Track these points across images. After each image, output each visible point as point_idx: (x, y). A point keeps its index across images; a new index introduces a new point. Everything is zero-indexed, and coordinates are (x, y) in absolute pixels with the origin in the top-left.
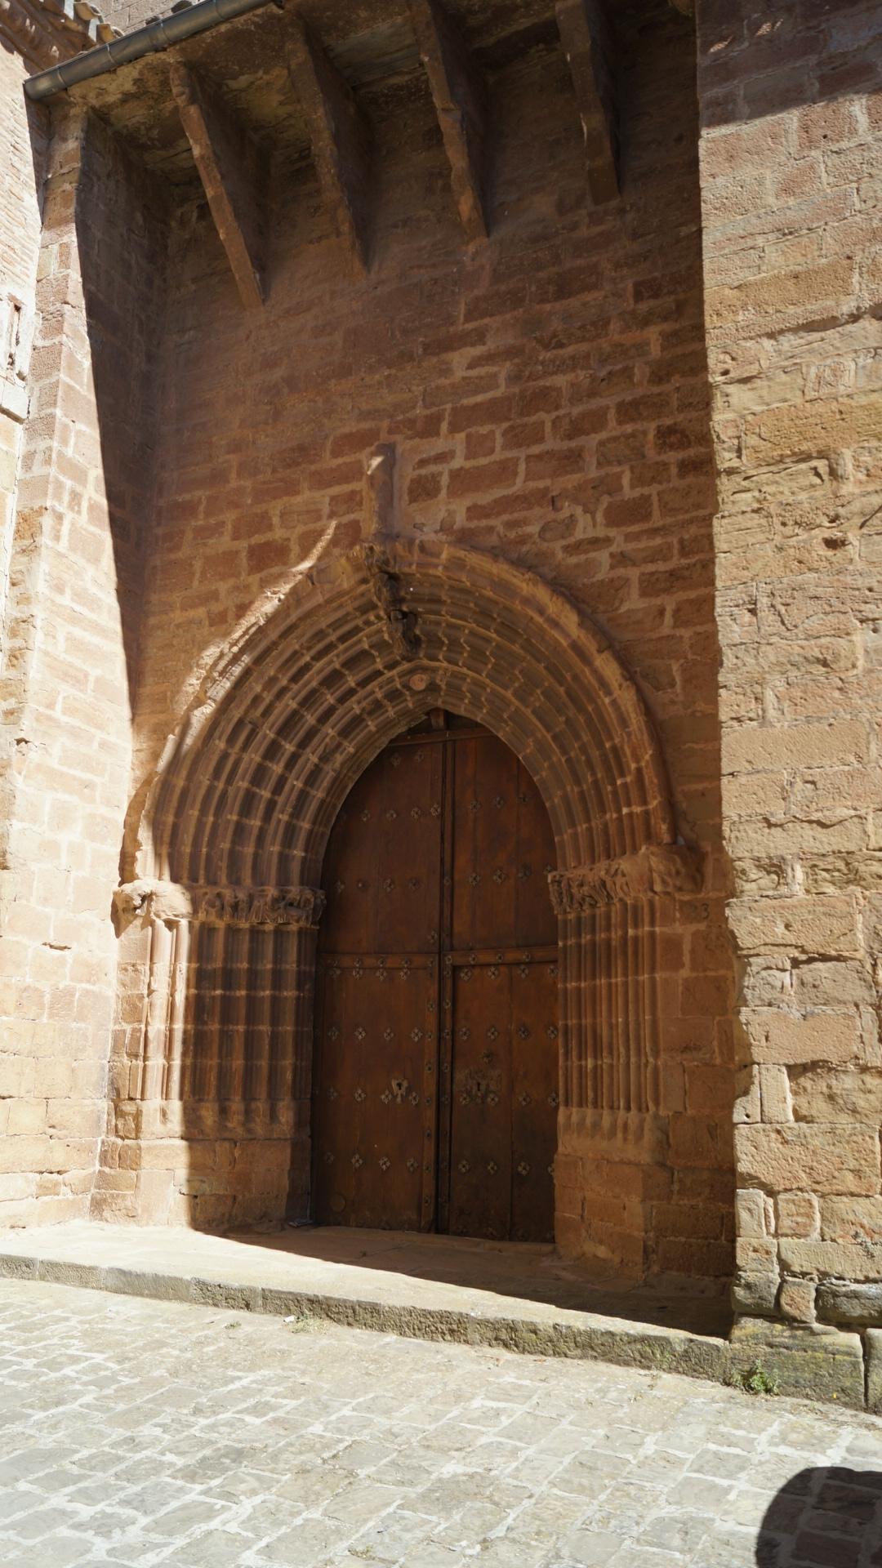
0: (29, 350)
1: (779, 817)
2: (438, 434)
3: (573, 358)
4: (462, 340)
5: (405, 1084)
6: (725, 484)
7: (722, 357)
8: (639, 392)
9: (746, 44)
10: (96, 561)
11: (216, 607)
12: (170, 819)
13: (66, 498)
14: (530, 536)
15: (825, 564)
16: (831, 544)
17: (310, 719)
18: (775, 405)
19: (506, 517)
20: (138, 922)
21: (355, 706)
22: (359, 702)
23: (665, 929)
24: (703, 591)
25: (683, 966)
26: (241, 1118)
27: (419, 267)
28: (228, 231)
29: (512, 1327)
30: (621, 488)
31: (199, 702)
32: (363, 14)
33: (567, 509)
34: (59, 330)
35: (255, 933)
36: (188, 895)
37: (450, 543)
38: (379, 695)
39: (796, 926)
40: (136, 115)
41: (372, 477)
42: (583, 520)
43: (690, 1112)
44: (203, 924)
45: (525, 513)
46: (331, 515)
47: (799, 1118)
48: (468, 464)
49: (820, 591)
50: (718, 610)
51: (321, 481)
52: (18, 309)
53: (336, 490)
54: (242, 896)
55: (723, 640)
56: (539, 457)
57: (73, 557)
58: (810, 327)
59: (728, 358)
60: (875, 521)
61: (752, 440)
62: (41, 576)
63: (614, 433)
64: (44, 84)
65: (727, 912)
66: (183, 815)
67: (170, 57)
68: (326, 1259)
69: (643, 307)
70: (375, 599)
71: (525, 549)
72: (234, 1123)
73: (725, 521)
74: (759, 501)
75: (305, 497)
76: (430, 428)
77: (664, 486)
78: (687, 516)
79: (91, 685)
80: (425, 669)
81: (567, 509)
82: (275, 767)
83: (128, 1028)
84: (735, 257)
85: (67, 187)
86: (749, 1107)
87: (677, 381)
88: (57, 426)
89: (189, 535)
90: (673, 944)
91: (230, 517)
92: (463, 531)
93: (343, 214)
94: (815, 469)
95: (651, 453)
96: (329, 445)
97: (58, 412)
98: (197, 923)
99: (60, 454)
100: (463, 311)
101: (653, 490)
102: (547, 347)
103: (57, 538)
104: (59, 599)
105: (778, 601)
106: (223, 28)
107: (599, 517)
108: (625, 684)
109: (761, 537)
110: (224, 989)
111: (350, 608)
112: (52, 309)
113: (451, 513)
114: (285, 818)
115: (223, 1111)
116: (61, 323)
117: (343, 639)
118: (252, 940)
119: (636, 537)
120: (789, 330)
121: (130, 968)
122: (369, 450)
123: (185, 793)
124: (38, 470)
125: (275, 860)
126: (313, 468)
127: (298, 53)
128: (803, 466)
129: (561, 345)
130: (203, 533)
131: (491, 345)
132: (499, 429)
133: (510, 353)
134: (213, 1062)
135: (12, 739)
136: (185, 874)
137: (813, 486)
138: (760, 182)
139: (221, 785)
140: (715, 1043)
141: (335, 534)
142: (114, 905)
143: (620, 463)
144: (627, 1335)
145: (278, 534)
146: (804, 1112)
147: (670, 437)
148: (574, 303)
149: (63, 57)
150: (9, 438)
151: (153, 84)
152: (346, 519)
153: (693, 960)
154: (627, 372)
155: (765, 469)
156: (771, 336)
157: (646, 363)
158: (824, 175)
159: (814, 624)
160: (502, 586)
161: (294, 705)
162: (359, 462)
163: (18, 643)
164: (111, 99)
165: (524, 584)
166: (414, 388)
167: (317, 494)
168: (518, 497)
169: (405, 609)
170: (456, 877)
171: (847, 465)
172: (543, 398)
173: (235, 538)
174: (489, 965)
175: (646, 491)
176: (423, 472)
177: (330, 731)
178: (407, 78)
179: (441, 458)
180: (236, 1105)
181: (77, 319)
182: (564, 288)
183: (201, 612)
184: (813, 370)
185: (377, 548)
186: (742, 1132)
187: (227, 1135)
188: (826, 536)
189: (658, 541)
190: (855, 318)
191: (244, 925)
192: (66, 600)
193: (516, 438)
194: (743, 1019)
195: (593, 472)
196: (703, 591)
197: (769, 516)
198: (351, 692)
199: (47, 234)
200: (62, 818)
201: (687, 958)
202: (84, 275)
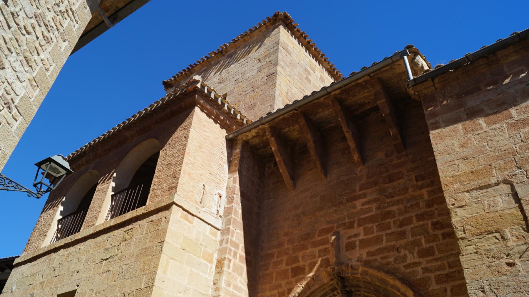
0: (223, 208)
2: (353, 228)
3: (397, 201)
6: (461, 243)
7: (451, 199)
8: (423, 211)
10: (241, 275)
11: (281, 290)
13: (232, 254)
14: (390, 262)
15: (509, 272)
16: (509, 265)
18: (474, 215)
19: (381, 255)
24: (460, 282)
28: (283, 170)
30: (422, 244)
32: (320, 110)
33: (403, 252)
34: (232, 202)
37: (362, 265)
40: (256, 141)
41: (332, 243)
45: (388, 254)
46: (319, 257)
48: (365, 238)
49: (509, 283)
50: (469, 291)
51: (315, 244)
52: (220, 197)
53: (320, 248)
56: (390, 234)
57: (234, 274)
58: (481, 188)
59: (453, 200)
60: (525, 255)
61: (469, 227)
62: (223, 281)
63: (416, 225)
64: (231, 136)
67: (266, 126)
69: (419, 183)
70: (336, 286)
71: (389, 267)
74: (476, 249)
75: (310, 250)
76: (351, 226)
77: (438, 243)
78: (448, 253)
81: (403, 252)
84: (449, 168)
85: (236, 162)
87: (436, 206)
88: (231, 231)
89: (271, 265)
91: (285, 258)
92: (366, 261)
93: (318, 162)
94: (495, 236)
95: (431, 231)
96: (317, 232)
97: (231, 227)
99: (231, 240)
101: (434, 244)
102: (388, 198)
103: (229, 268)
104: (229, 289)
105: (493, 288)
106: (281, 117)
107: (415, 254)
109: (480, 262)
112: (230, 196)
116: (233, 200)
120: (474, 189)
124: (224, 245)
126: (312, 240)
127: (302, 121)
128: (490, 236)
129: (392, 197)
131: (369, 198)
132: (375, 225)
133: (375, 200)
137: (496, 243)
138: (453, 145)
141: (321, 263)
145: (301, 263)
147: (436, 225)
148: (395, 183)
149: (236, 128)
150: (215, 236)
151: (261, 133)
152: (324, 258)
154: (417, 204)
155: (476, 237)
156: (467, 192)
157: (424, 201)
158: (474, 141)
160: (382, 281)
162: (328, 238)
164: (249, 138)
165: (391, 280)
167: (314, 249)
168: (384, 248)
171: (508, 235)
172: (389, 214)
173: (287, 265)
175: (431, 244)
176: (350, 240)
179: (356, 235)
181: (238, 198)
182: (391, 179)
184: (486, 202)
185: (336, 268)
188: (506, 262)
189: (439, 263)
190: (497, 184)
192: (231, 289)
193: (381, 228)
195: (410, 239)
196: (460, 282)
197: (481, 254)
199: (230, 175)
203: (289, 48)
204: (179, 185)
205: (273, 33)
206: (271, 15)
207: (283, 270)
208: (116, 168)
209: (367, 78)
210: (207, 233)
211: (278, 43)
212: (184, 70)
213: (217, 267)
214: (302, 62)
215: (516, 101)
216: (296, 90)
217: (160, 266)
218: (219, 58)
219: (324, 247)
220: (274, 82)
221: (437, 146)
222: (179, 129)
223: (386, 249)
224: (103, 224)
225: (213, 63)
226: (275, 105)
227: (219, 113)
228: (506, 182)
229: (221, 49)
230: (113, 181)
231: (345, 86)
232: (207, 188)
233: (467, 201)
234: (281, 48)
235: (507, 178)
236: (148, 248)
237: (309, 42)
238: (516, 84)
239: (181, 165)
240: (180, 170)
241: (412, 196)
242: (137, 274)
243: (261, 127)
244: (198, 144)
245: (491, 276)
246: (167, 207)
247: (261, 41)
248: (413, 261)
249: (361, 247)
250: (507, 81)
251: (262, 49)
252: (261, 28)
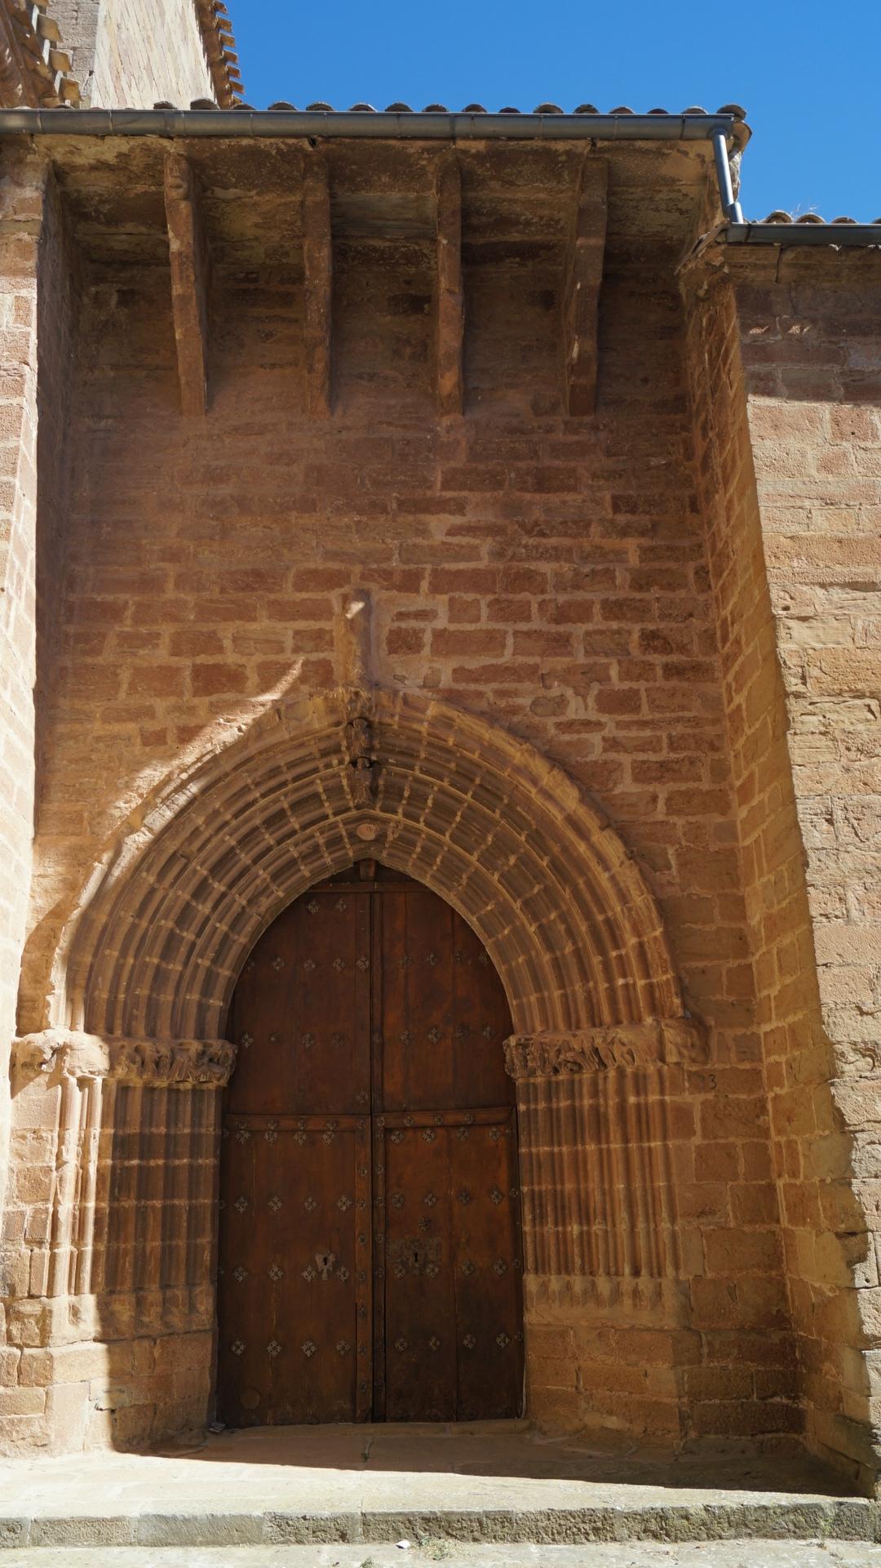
2: (417, 591)
3: (555, 549)
4: (441, 506)
5: (331, 1258)
8: (622, 594)
9: (779, 337)
11: (151, 726)
14: (521, 708)
18: (831, 646)
19: (495, 685)
20: (43, 1080)
22: (296, 845)
23: (677, 1099)
25: (694, 1133)
26: (159, 1309)
27: (389, 424)
29: (662, 1516)
30: (609, 678)
32: (385, 179)
33: (556, 690)
36: (106, 1049)
40: (101, 184)
41: (352, 620)
43: (710, 1275)
45: (514, 686)
46: (297, 650)
48: (453, 627)
51: (282, 612)
53: (301, 625)
58: (854, 586)
63: (600, 627)
66: (102, 956)
67: (172, 147)
68: (283, 1464)
69: (622, 519)
71: (515, 719)
73: (797, 738)
75: (263, 624)
76: (410, 583)
77: (650, 685)
78: (674, 715)
80: (374, 820)
82: (200, 907)
83: (28, 1209)
86: (868, 1272)
87: (655, 592)
89: (112, 641)
90: (683, 1113)
91: (167, 630)
92: (450, 691)
93: (321, 353)
98: (113, 1082)
100: (439, 478)
101: (641, 685)
102: (529, 533)
105: (850, 815)
106: (245, 142)
107: (591, 701)
108: (627, 863)
109: (830, 757)
110: (141, 1158)
115: (140, 1303)
119: (627, 726)
120: (837, 584)
121: (29, 1135)
125: (194, 1010)
126: (272, 596)
128: (858, 702)
129: (542, 534)
130: (130, 642)
132: (484, 600)
136: (102, 1025)
140: (729, 1207)
142: (13, 1057)
143: (606, 655)
144: (780, 1506)
145: (231, 658)
148: (554, 499)
151: (137, 163)
152: (314, 657)
153: (704, 1128)
154: (609, 574)
155: (827, 699)
156: (823, 586)
160: (491, 751)
164: (79, 160)
165: (516, 753)
166: (389, 541)
168: (507, 668)
169: (374, 758)
170: (387, 1034)
172: (528, 580)
174: (424, 1127)
175: (634, 685)
176: (403, 625)
178: (387, 244)
179: (421, 615)
180: (153, 1294)
183: (131, 727)
185: (364, 694)
187: (143, 1331)
193: (502, 611)
194: (855, 1189)
195: (581, 659)
197: (834, 740)
201: (698, 1126)
207: (160, 667)
209: (582, 147)
231: (510, 138)
233: (820, 609)
241: (597, 547)
243: (152, 140)
245: (849, 789)
248: (582, 715)
249: (436, 651)
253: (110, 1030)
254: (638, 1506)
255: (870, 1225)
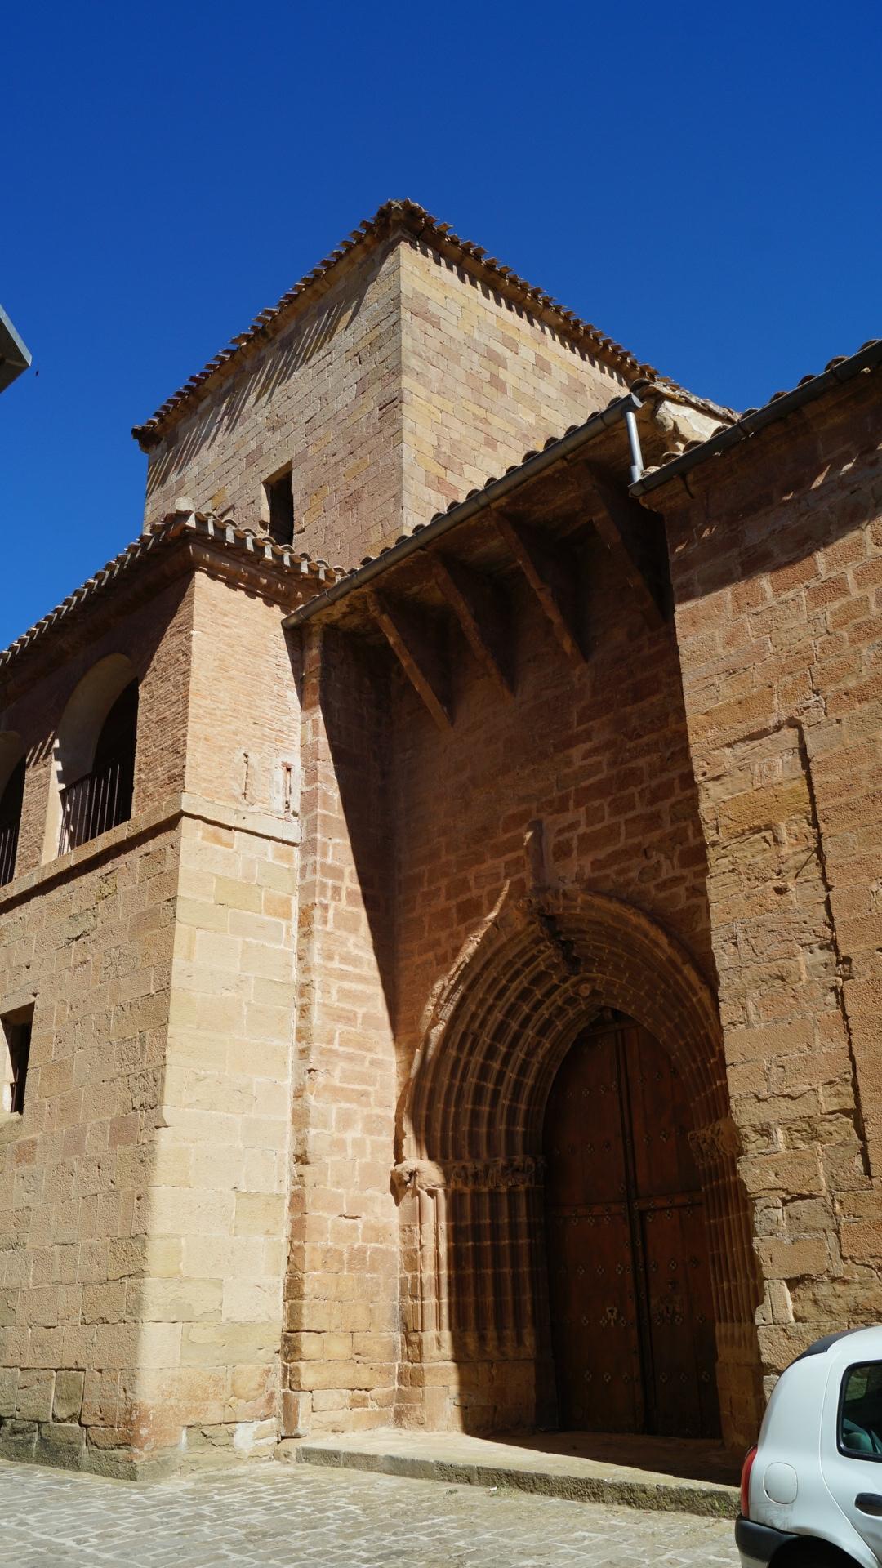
1: (764, 1094)
6: (711, 853)
10: (355, 930)
11: (440, 951)
12: (424, 1113)
13: (329, 893)
16: (780, 891)
17: (515, 1026)
19: (616, 867)
20: (409, 1193)
21: (545, 1012)
26: (495, 1343)
28: (420, 684)
30: (687, 838)
31: (434, 1023)
33: (656, 856)
34: (315, 779)
35: (494, 1195)
38: (560, 1002)
39: (782, 1174)
40: (354, 621)
41: (527, 847)
42: (666, 864)
44: (455, 1191)
46: (506, 877)
47: (798, 1319)
48: (588, 830)
49: (774, 926)
50: (714, 945)
51: (498, 851)
52: (289, 770)
54: (480, 1167)
55: (718, 967)
57: (338, 933)
58: (752, 737)
60: (803, 873)
61: (725, 821)
64: (293, 621)
65: (739, 1167)
66: (429, 1110)
67: (366, 590)
71: (630, 889)
72: (491, 1346)
76: (562, 807)
79: (359, 1021)
80: (588, 980)
81: (656, 856)
83: (409, 1275)
88: (319, 845)
89: (419, 900)
91: (443, 883)
92: (590, 880)
97: (319, 836)
99: (323, 864)
102: (630, 739)
103: (325, 922)
104: (330, 965)
107: (675, 861)
109: (736, 889)
111: (526, 943)
113: (581, 867)
114: (506, 1102)
115: (482, 1339)
117: (527, 964)
118: (509, 1201)
122: (526, 826)
123: (432, 1091)
124: (309, 877)
128: (757, 836)
129: (640, 736)
133: (609, 745)
134: (471, 1299)
135: (304, 1069)
136: (438, 1154)
139: (457, 1083)
145: (475, 893)
146: (800, 1315)
150: (289, 858)
156: (729, 745)
159: (773, 951)
161: (500, 1017)
163: (305, 1001)
171: (784, 835)
172: (632, 777)
174: (664, 1208)
176: (561, 838)
177: (530, 1032)
179: (573, 826)
180: (491, 1333)
181: (327, 767)
183: (431, 955)
186: (762, 1331)
190: (778, 728)
191: (485, 1190)
192: (336, 964)
193: (619, 807)
195: (669, 828)
197: (740, 874)
198: (540, 1003)
200: (346, 1121)
202: (330, 737)
203: (433, 308)
204: (187, 769)
205: (385, 266)
206: (370, 217)
208: (55, 727)
209: (560, 464)
210: (270, 858)
211: (397, 302)
212: (179, 394)
213: (301, 924)
214: (476, 335)
215: (828, 533)
216: (463, 429)
217: (176, 948)
218: (259, 350)
219: (514, 855)
220: (397, 427)
221: (688, 641)
222: (169, 632)
223: (627, 853)
224: (55, 863)
225: (248, 364)
226: (405, 495)
227: (254, 571)
228: (794, 723)
229: (260, 325)
230: (57, 759)
231: (516, 487)
232: (253, 759)
234: (406, 315)
235: (795, 715)
236: (151, 911)
237: (490, 267)
238: (833, 491)
239: (184, 721)
240: (184, 735)
242: (138, 966)
244: (216, 663)
246: (172, 823)
247: (356, 294)
248: (672, 874)
250: (819, 481)
251: (362, 321)
252: (352, 255)
253: (445, 1157)
254: (618, 1480)
255: (767, 1275)
